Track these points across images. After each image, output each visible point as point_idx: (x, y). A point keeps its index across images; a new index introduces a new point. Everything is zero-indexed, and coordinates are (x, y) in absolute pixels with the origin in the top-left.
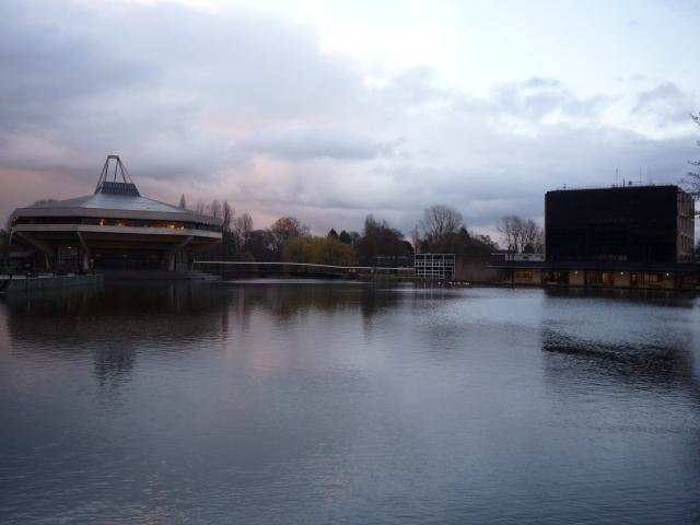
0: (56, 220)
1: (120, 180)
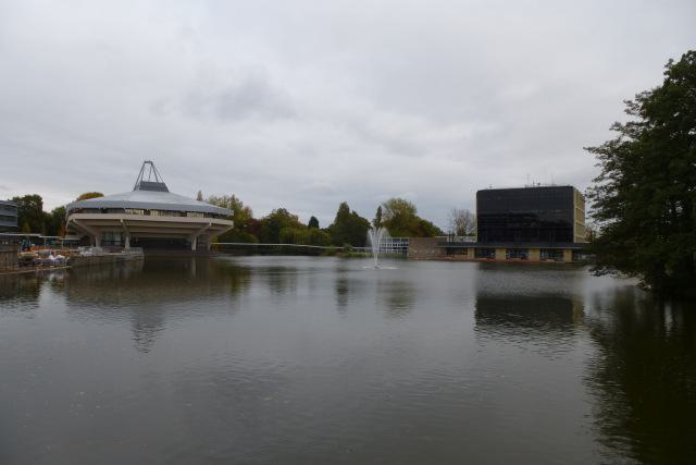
1: (153, 180)
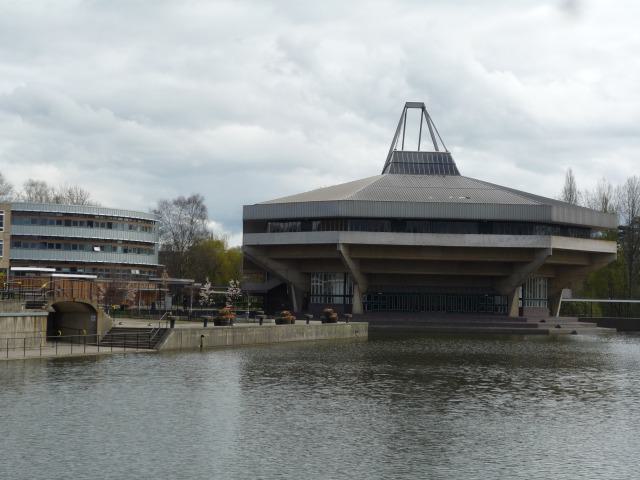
0: (306, 224)
1: (427, 147)
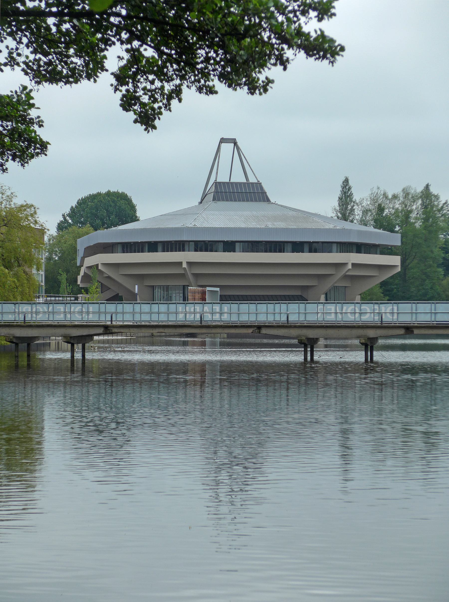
1: (238, 177)
